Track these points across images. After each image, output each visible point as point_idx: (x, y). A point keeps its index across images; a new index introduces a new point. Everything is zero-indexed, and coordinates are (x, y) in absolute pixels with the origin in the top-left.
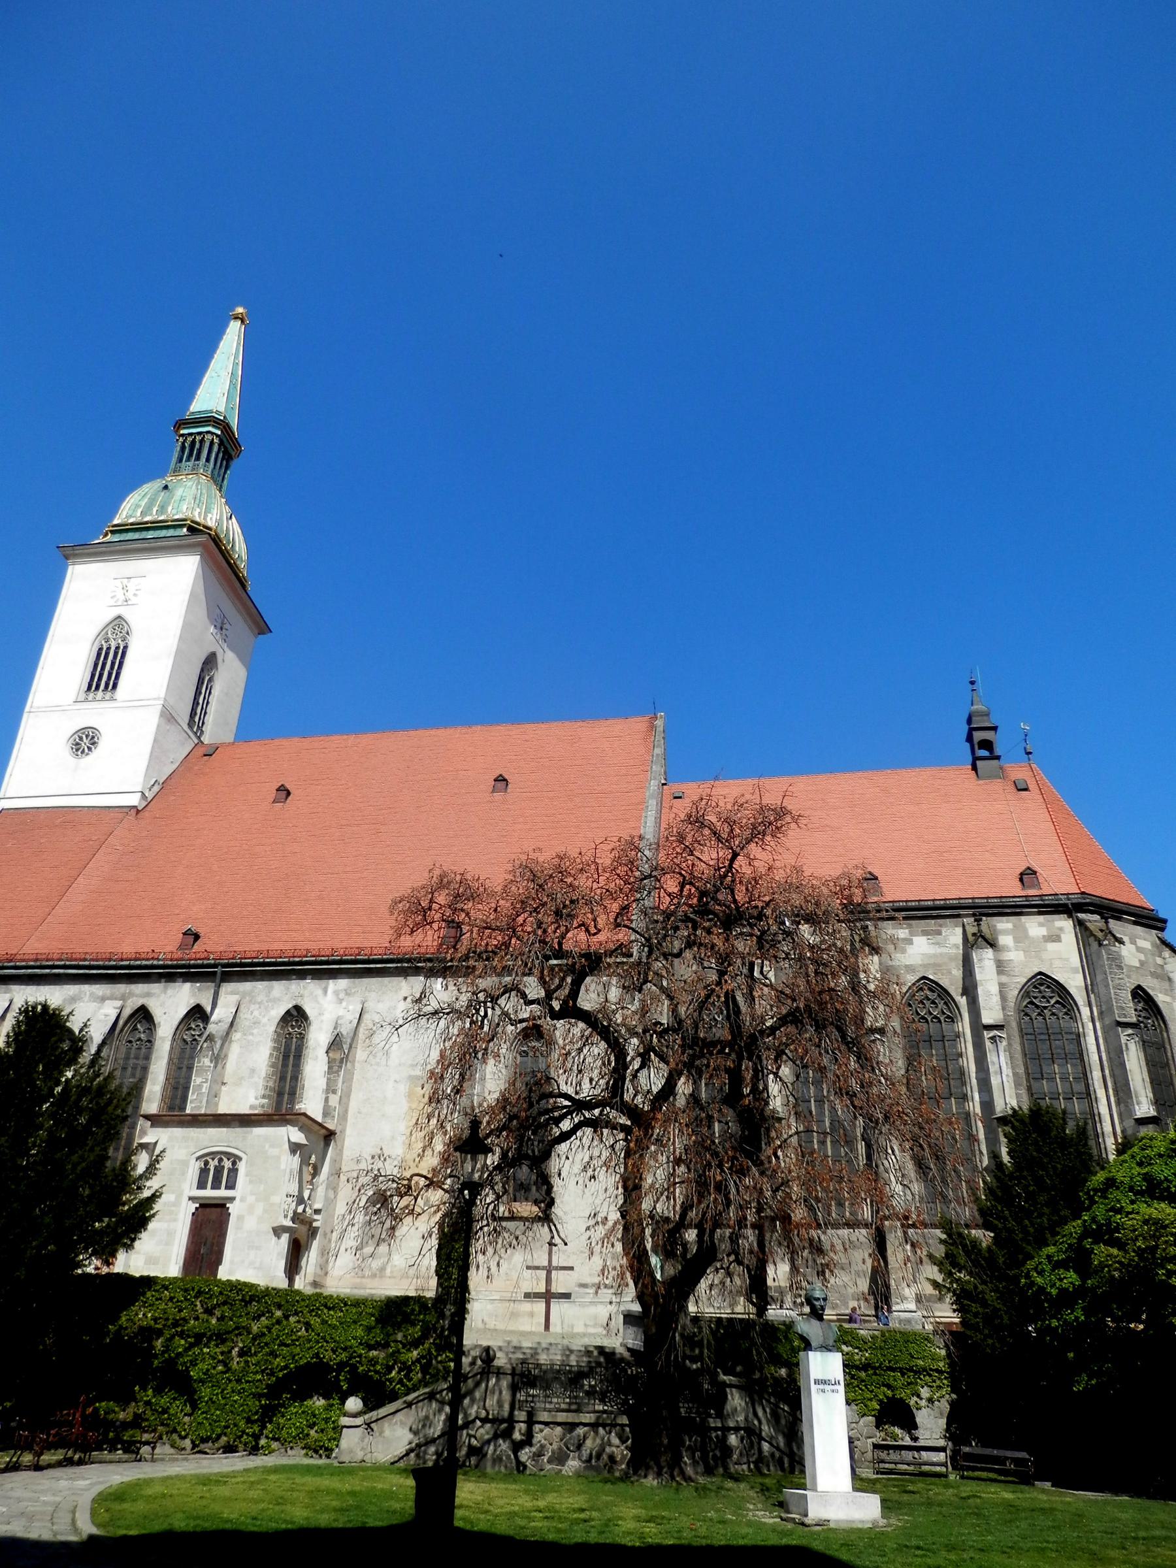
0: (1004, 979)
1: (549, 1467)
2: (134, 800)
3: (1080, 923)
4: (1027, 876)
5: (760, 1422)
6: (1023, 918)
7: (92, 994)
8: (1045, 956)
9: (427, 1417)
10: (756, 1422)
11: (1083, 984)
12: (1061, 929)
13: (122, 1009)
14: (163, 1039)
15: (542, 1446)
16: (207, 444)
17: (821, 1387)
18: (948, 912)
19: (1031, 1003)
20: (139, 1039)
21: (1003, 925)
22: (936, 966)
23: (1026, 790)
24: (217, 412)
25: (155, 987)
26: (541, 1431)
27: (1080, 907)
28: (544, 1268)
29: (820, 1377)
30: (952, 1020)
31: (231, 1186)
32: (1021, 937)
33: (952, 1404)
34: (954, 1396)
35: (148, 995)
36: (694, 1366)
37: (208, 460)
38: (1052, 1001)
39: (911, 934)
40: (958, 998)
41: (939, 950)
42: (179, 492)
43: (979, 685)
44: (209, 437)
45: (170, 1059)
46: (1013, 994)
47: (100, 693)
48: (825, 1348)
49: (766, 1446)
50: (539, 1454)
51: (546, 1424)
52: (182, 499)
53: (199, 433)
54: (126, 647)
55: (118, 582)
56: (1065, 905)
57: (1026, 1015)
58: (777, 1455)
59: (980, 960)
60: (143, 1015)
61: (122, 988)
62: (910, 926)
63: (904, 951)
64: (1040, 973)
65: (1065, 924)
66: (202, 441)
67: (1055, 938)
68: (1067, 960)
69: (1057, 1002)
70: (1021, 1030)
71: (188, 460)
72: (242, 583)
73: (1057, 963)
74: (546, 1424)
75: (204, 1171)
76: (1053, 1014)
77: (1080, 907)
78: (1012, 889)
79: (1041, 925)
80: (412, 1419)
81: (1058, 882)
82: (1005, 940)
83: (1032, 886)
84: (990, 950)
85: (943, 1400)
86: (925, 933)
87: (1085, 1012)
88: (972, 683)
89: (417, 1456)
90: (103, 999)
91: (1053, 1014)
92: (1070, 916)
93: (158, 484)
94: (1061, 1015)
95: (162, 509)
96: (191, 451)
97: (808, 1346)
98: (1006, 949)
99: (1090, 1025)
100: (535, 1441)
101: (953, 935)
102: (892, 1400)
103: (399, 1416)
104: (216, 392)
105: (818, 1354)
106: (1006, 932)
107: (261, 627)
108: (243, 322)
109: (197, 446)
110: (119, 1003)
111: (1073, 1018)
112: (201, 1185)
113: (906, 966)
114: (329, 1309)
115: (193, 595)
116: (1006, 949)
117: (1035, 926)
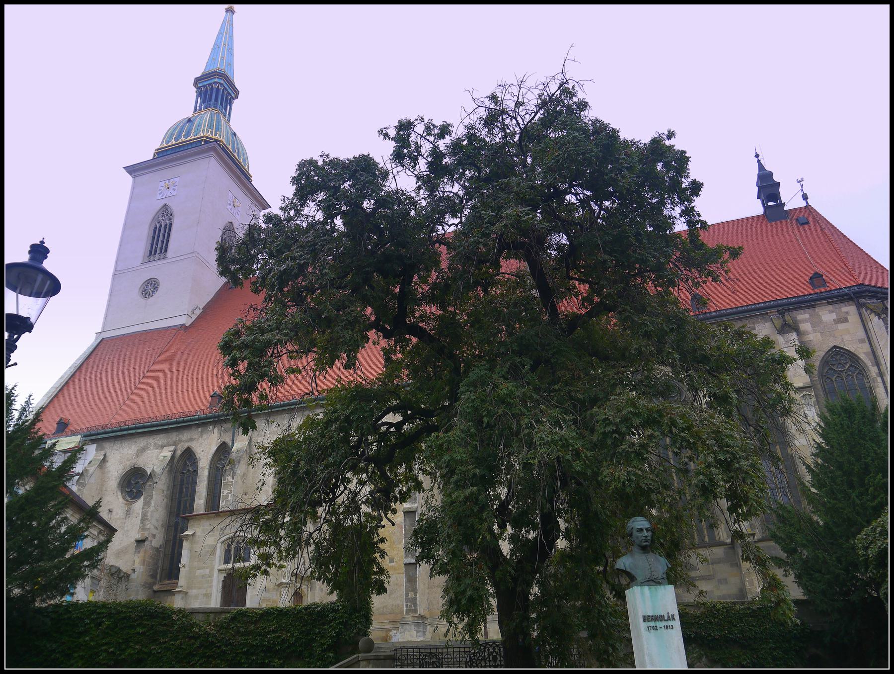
2: (187, 321)
4: (817, 278)
7: (155, 444)
11: (870, 350)
13: (175, 451)
14: (203, 468)
16: (214, 90)
17: (652, 624)
19: (831, 369)
20: (189, 471)
23: (807, 223)
25: (195, 433)
29: (650, 613)
32: (816, 323)
35: (191, 440)
37: (216, 100)
45: (209, 481)
47: (157, 256)
48: (653, 581)
53: (209, 85)
54: (171, 224)
56: (848, 294)
60: (189, 455)
61: (174, 436)
64: (835, 347)
65: (850, 309)
75: (228, 552)
78: (806, 290)
82: (805, 327)
90: (162, 447)
97: (632, 579)
105: (646, 589)
106: (805, 321)
109: (209, 93)
110: (172, 448)
112: (227, 561)
117: (827, 314)
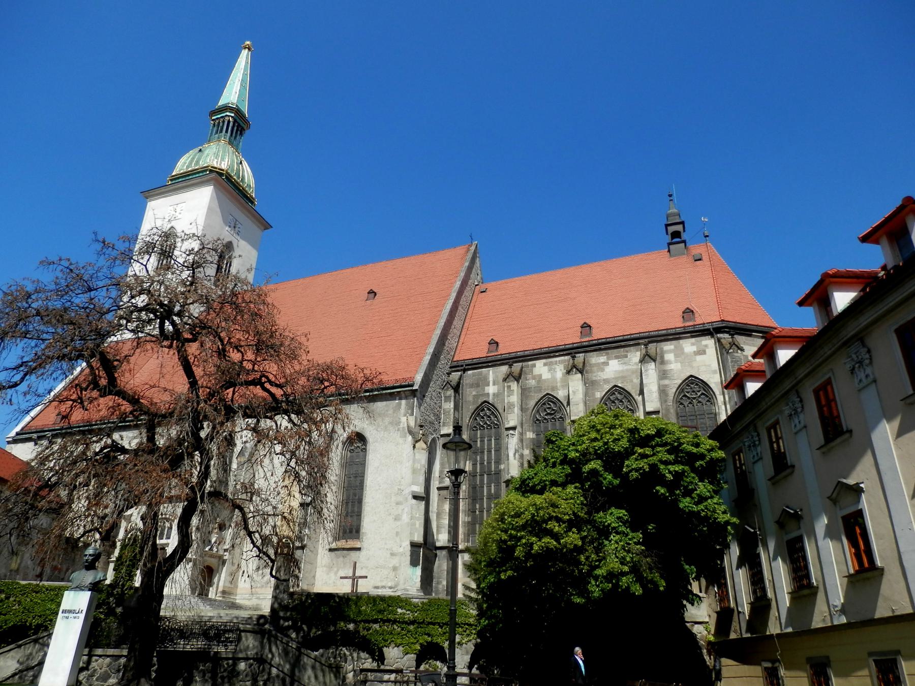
0: (666, 382)
1: (96, 683)
3: (719, 340)
5: (273, 656)
6: (681, 341)
8: (695, 364)
9: (31, 654)
10: (270, 656)
12: (706, 346)
15: (95, 670)
17: (67, 615)
18: (632, 343)
21: (668, 347)
22: (623, 378)
23: (700, 260)
24: (232, 104)
26: (97, 661)
27: (718, 330)
28: (350, 578)
30: (633, 411)
31: (168, 538)
32: (679, 353)
33: (476, 645)
34: (479, 640)
36: (286, 624)
37: (227, 132)
38: (699, 394)
39: (608, 359)
40: (636, 397)
41: (626, 367)
42: (206, 152)
43: (675, 197)
44: (227, 118)
46: (672, 391)
49: (274, 671)
50: (92, 676)
51: (100, 656)
52: (208, 155)
55: (171, 208)
56: (709, 330)
57: (682, 404)
58: (282, 675)
59: (646, 371)
62: (607, 354)
63: (603, 370)
64: (691, 376)
65: (709, 343)
66: (223, 122)
67: (702, 352)
68: (709, 366)
69: (703, 394)
70: (677, 414)
71: (217, 133)
72: (250, 200)
73: (703, 369)
74: (100, 656)
76: (699, 402)
77: (718, 330)
78: (676, 322)
79: (693, 344)
80: (20, 655)
81: (707, 315)
82: (669, 357)
83: (690, 320)
84: (653, 363)
85: (469, 643)
86: (617, 357)
87: (720, 398)
88: (670, 196)
89: (20, 678)
91: (699, 402)
92: (712, 336)
93: (197, 150)
94: (704, 402)
95: (197, 162)
96: (218, 127)
98: (669, 362)
99: (723, 407)
100: (91, 667)
101: (635, 356)
102: (430, 644)
103: (12, 653)
104: (233, 92)
106: (670, 351)
107: (266, 226)
108: (249, 49)
111: (713, 404)
113: (604, 380)
114: (37, 593)
115: (210, 209)
116: (669, 362)
117: (689, 346)
